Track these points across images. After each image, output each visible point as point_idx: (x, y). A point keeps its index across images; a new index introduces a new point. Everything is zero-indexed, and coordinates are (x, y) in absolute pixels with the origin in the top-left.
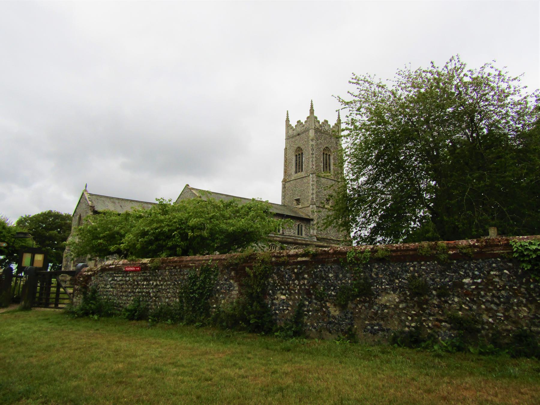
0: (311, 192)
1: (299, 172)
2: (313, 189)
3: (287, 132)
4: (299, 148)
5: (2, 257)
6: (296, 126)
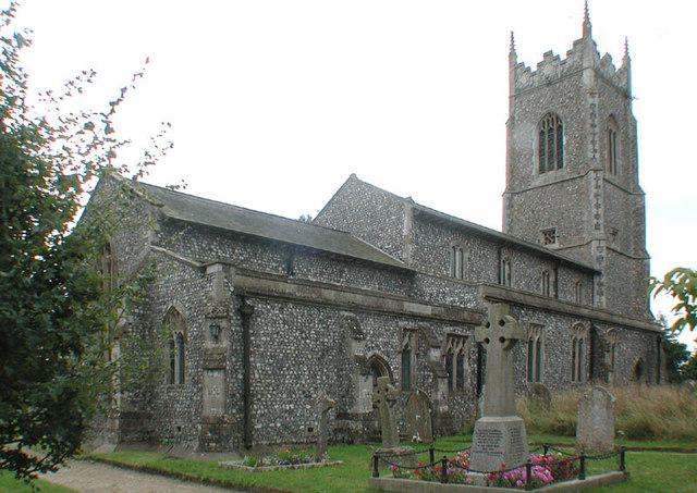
0: (591, 146)
1: (551, 169)
2: (593, 126)
3: (514, 79)
4: (549, 114)
5: (3, 461)
6: (539, 65)
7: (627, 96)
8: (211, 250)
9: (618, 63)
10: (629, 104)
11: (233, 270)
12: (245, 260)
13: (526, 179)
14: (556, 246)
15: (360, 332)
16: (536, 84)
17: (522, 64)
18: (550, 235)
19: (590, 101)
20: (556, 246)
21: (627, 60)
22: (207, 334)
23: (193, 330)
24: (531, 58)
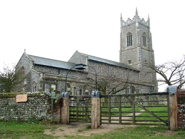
0: (138, 40)
1: (130, 45)
4: (129, 32)
7: (149, 28)
8: (43, 69)
9: (146, 20)
10: (149, 29)
11: (44, 74)
12: (50, 71)
13: (124, 48)
14: (131, 64)
15: (70, 86)
16: (126, 25)
17: (123, 21)
18: (130, 61)
19: (137, 30)
20: (131, 64)
21: (149, 19)
22: (40, 86)
23: (37, 85)
24: (125, 19)
